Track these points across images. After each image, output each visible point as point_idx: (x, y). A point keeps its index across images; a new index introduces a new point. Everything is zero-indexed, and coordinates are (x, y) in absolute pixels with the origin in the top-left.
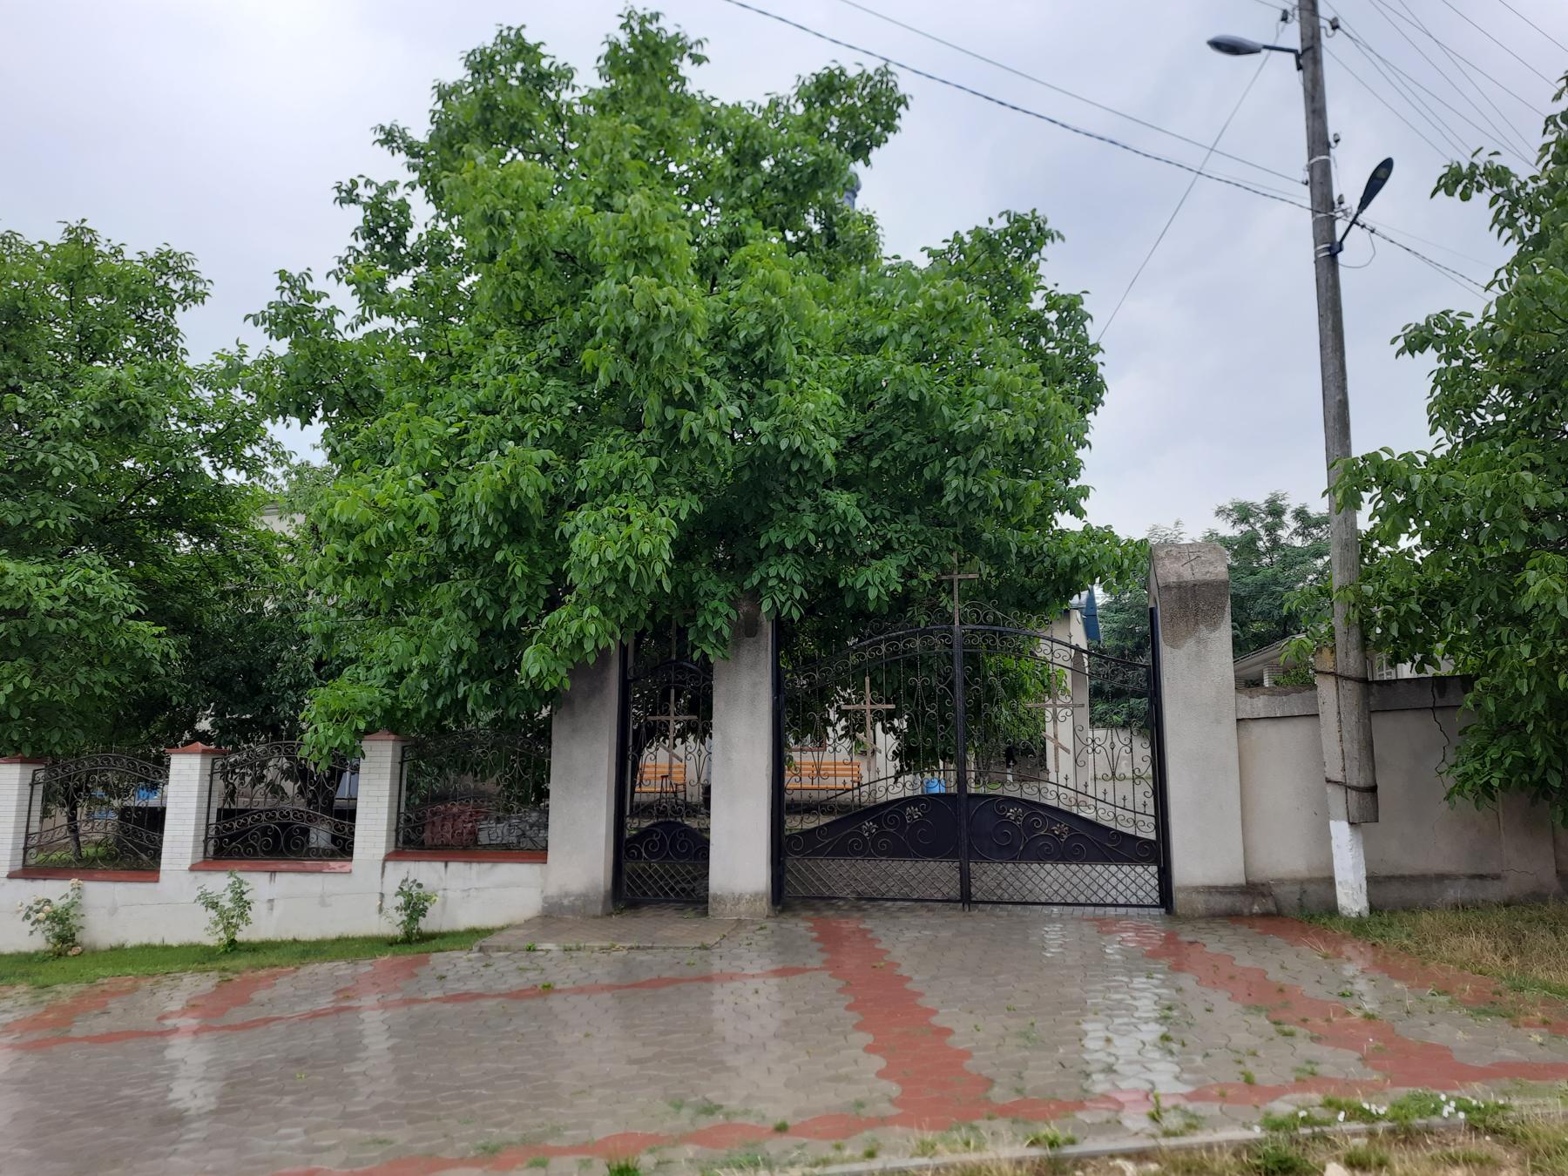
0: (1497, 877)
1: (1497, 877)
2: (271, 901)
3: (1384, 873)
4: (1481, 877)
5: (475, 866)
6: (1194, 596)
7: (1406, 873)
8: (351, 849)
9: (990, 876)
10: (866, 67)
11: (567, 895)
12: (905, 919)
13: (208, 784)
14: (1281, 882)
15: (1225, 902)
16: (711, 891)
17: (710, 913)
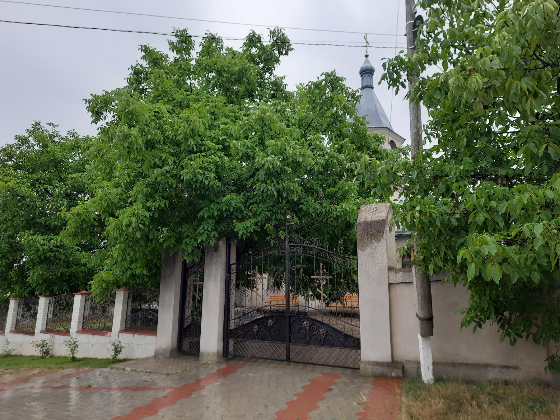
0: (516, 368)
1: (516, 368)
2: (93, 344)
3: (458, 361)
4: (507, 367)
5: (141, 336)
6: (371, 228)
7: (470, 362)
8: (112, 329)
9: (295, 349)
10: (271, 29)
11: (161, 349)
12: (273, 365)
13: (84, 304)
14: (409, 362)
15: (379, 370)
16: (201, 351)
17: (200, 359)
